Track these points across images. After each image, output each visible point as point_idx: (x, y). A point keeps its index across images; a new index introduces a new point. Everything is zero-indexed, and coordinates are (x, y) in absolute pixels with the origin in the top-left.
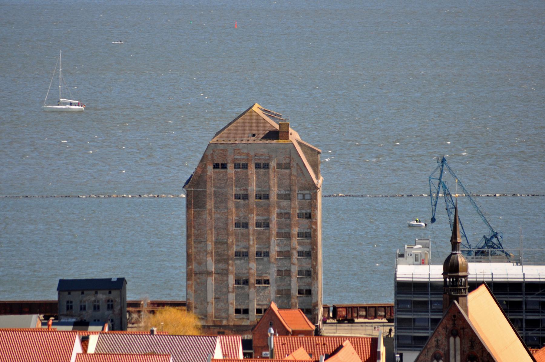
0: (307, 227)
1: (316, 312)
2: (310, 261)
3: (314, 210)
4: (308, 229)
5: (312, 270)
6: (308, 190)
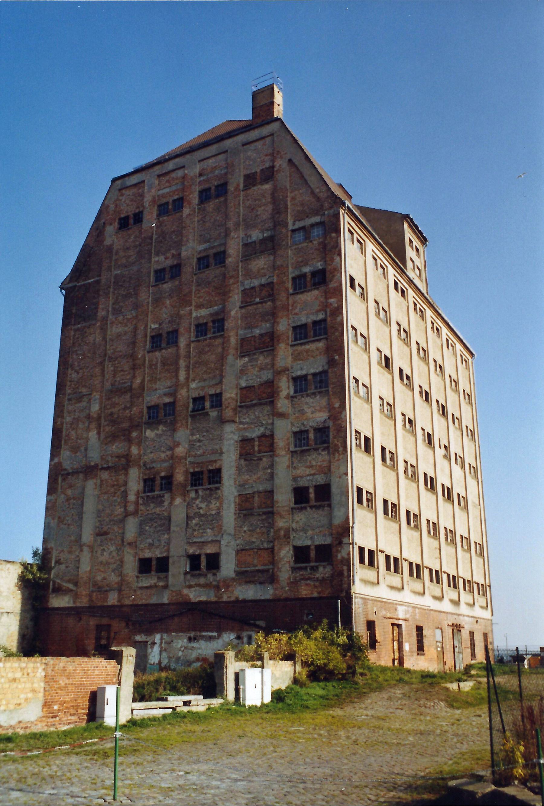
0: (317, 307)
1: (344, 554)
2: (324, 402)
3: (332, 260)
4: (318, 311)
5: (331, 424)
6: (317, 214)
